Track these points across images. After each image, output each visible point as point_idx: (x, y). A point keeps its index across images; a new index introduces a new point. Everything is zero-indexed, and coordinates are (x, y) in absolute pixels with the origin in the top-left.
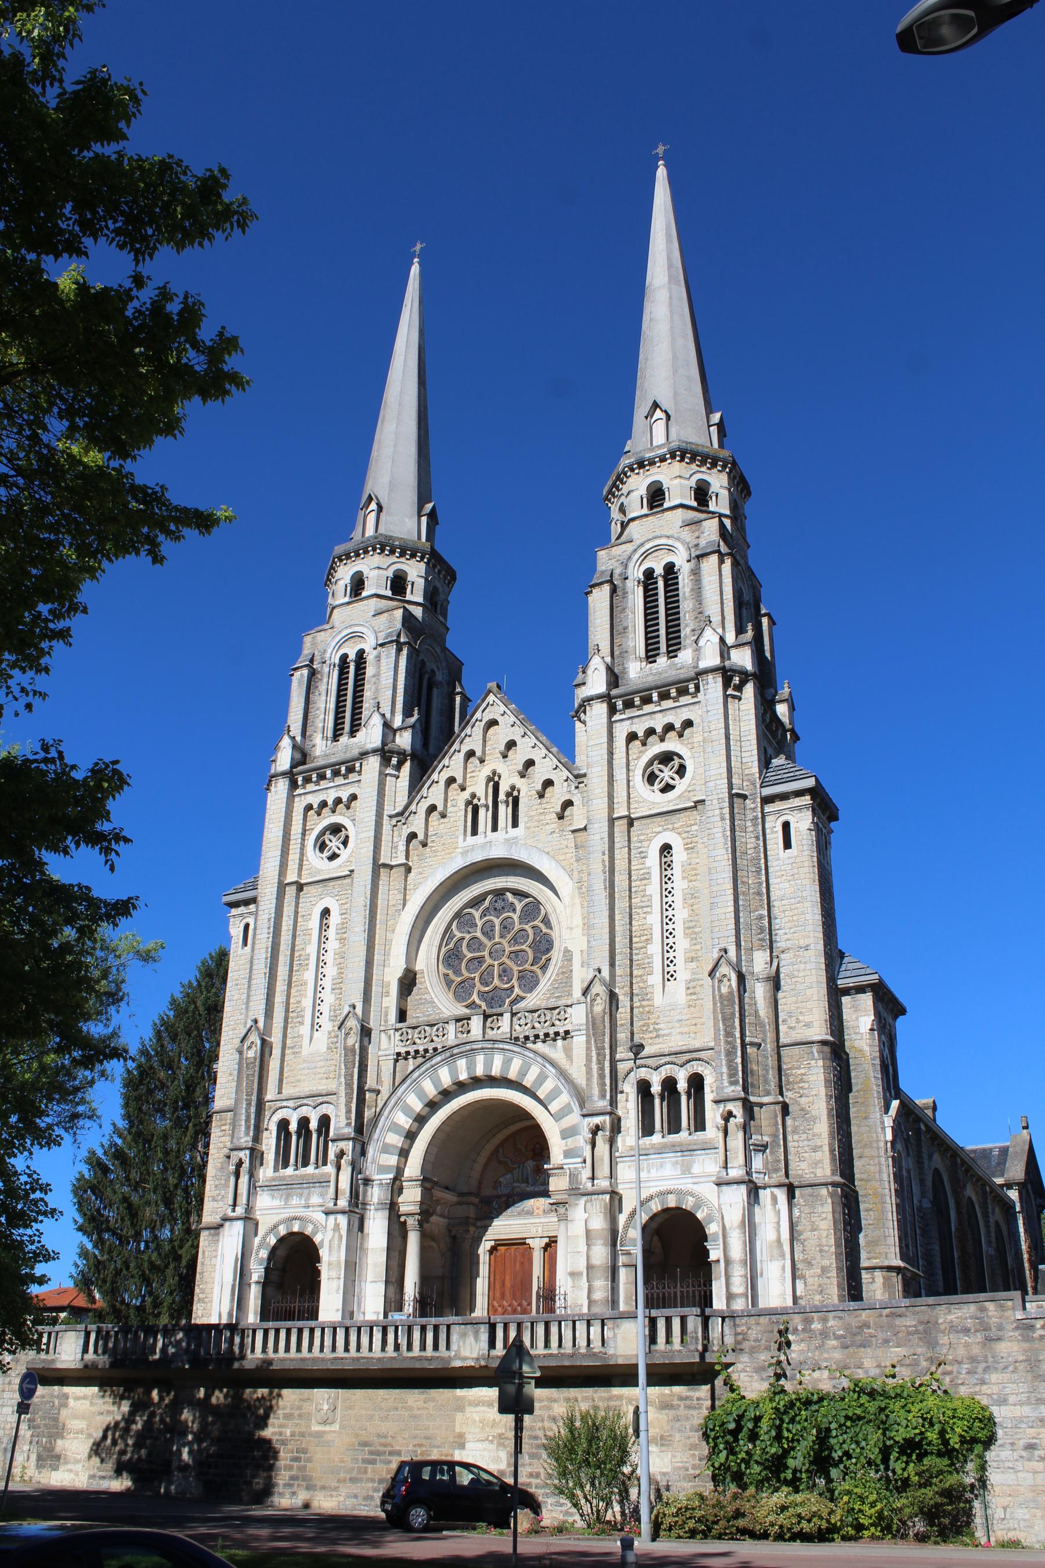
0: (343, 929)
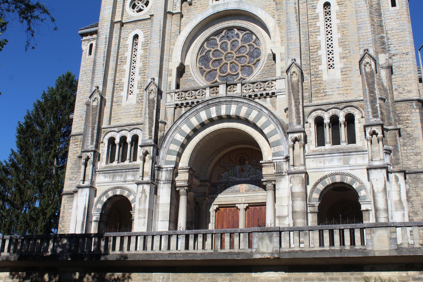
0: (146, 44)
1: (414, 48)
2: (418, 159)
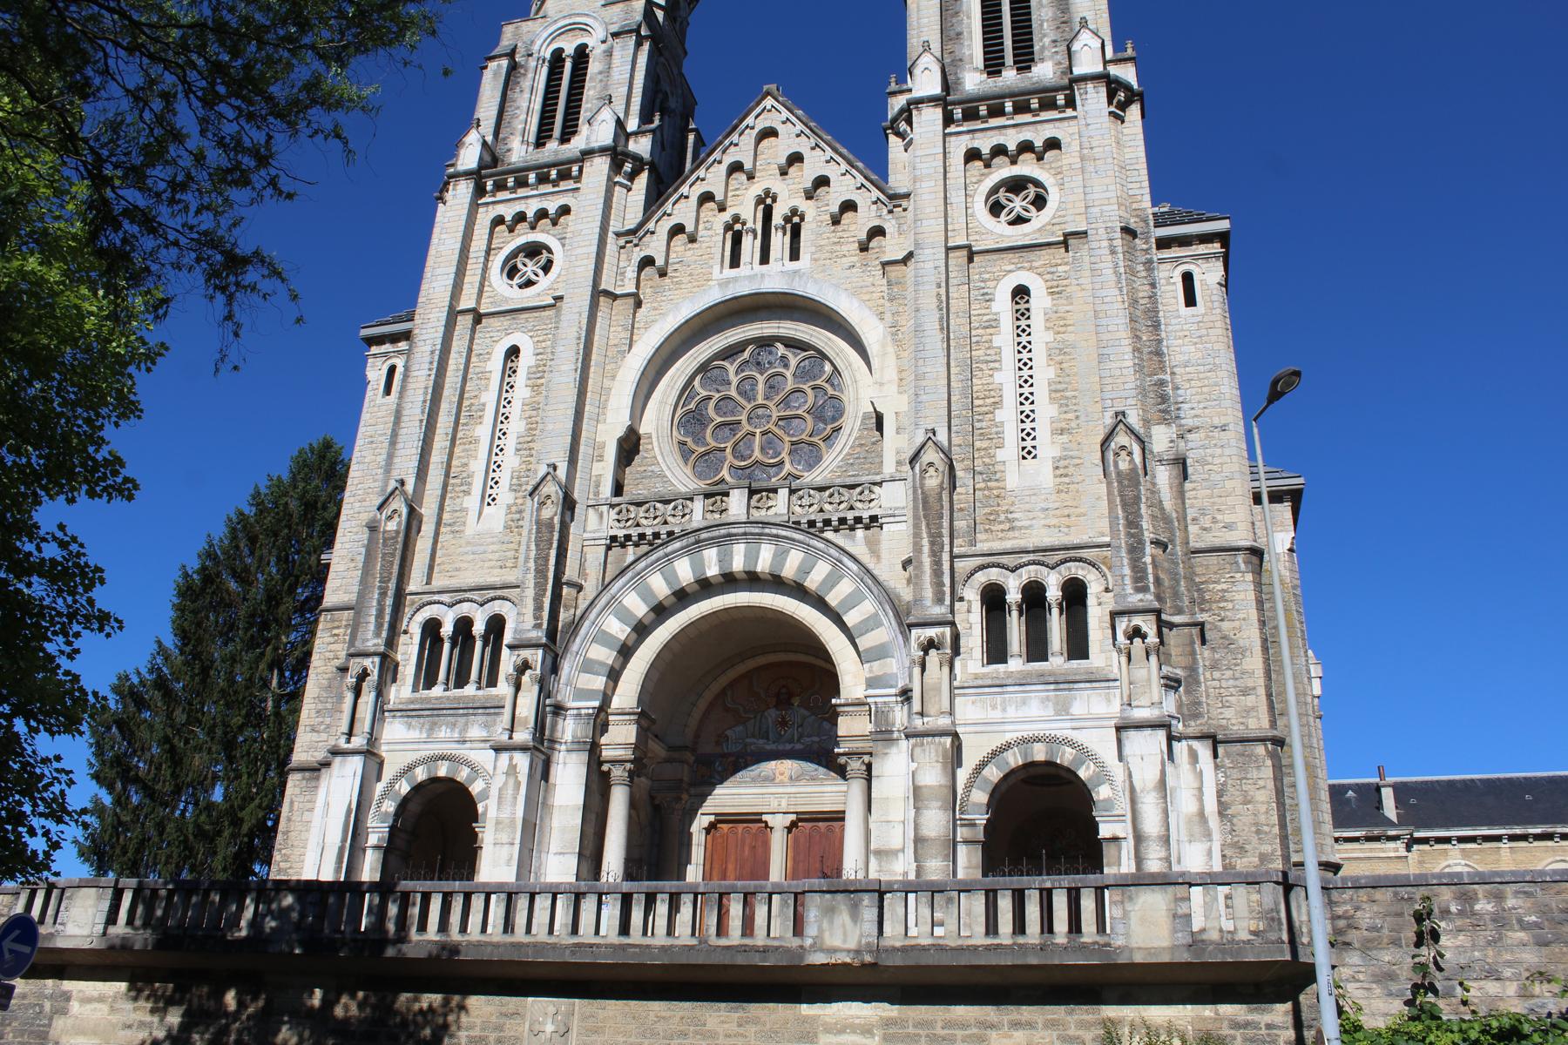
1: (1240, 415)
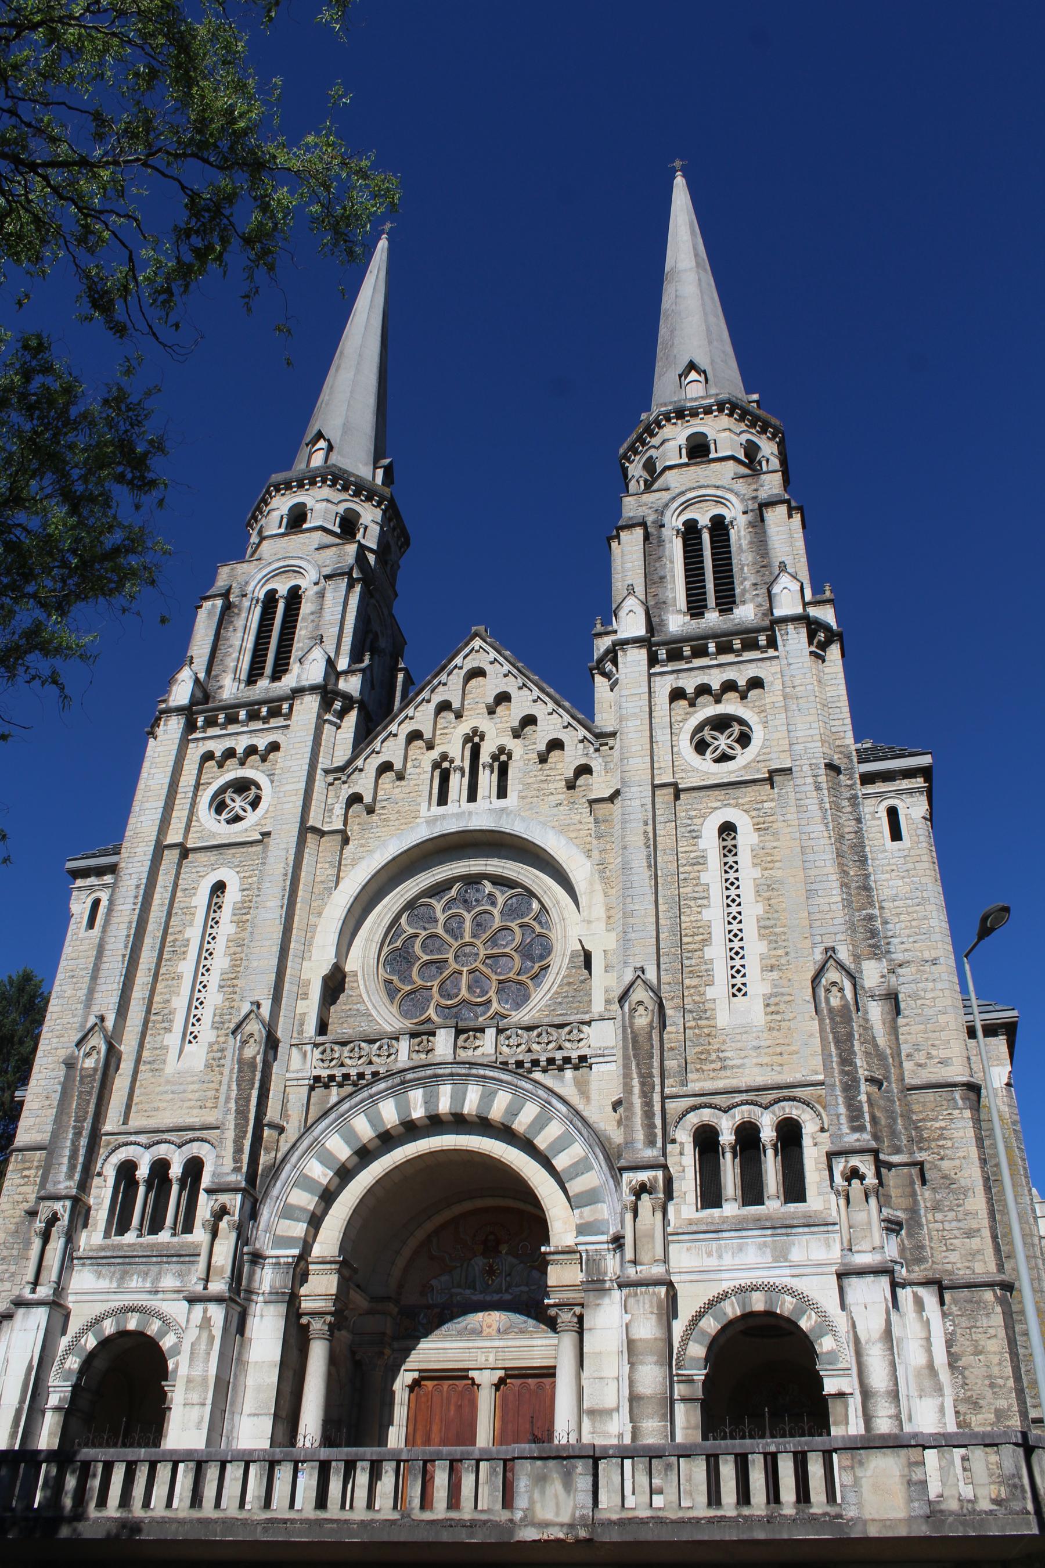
0: (244, 909)
1: (950, 948)
2: (974, 1247)
